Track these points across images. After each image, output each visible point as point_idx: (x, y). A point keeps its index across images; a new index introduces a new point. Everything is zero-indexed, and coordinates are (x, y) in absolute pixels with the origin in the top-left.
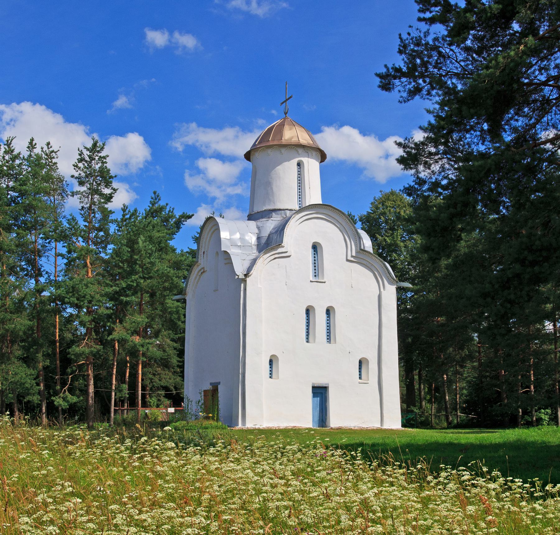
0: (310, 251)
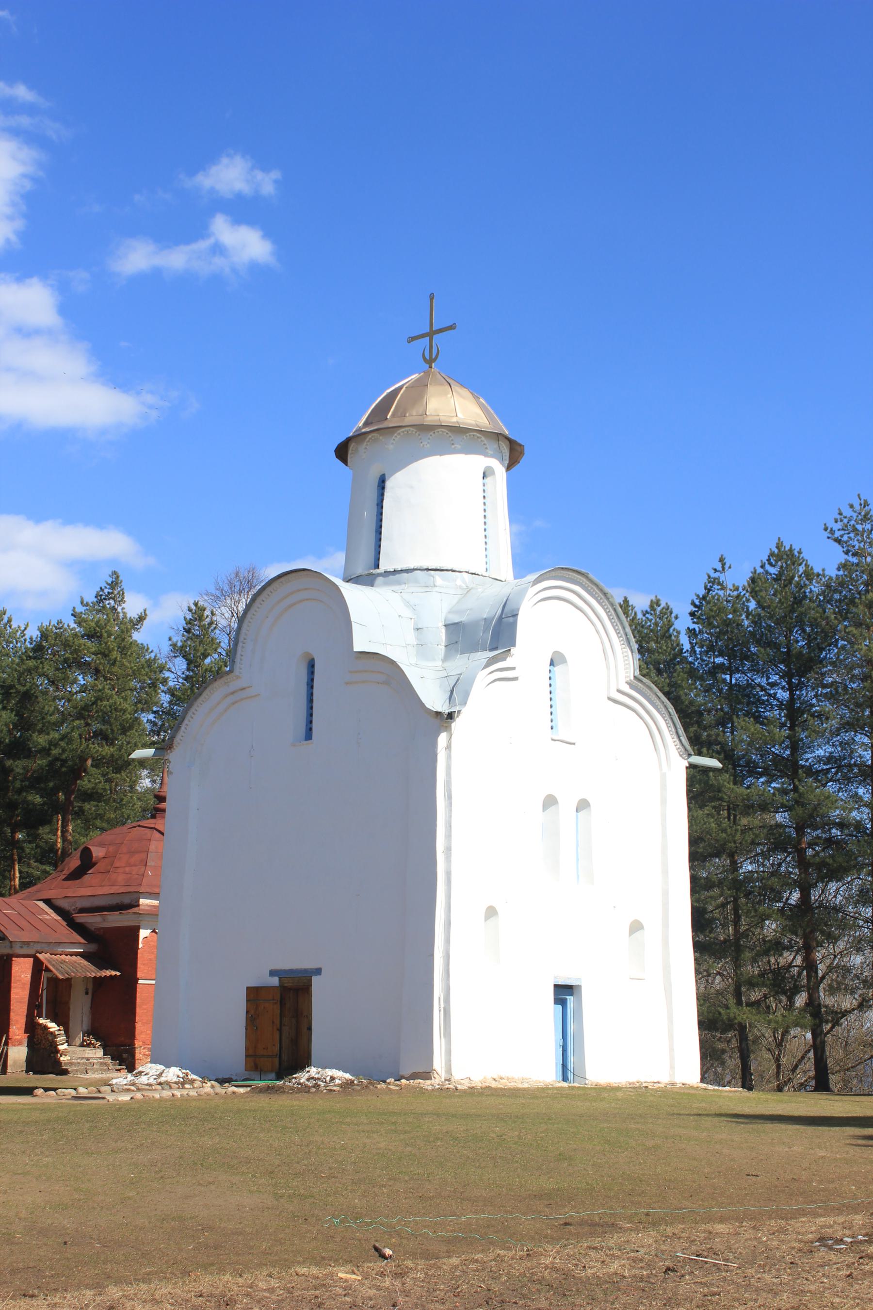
0: (550, 994)
